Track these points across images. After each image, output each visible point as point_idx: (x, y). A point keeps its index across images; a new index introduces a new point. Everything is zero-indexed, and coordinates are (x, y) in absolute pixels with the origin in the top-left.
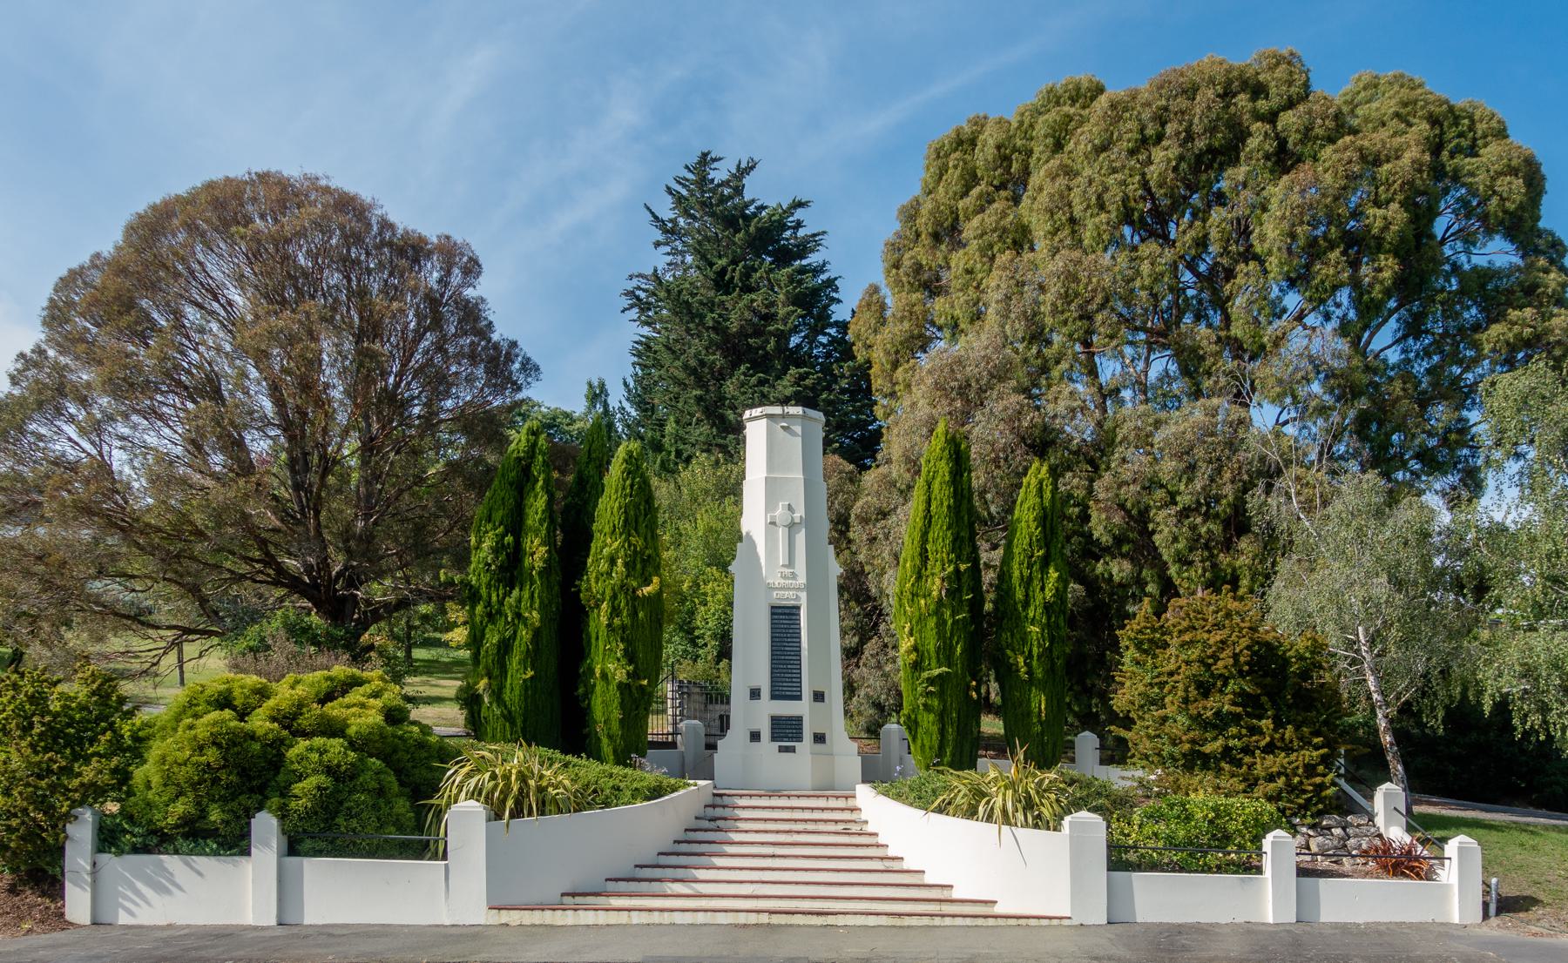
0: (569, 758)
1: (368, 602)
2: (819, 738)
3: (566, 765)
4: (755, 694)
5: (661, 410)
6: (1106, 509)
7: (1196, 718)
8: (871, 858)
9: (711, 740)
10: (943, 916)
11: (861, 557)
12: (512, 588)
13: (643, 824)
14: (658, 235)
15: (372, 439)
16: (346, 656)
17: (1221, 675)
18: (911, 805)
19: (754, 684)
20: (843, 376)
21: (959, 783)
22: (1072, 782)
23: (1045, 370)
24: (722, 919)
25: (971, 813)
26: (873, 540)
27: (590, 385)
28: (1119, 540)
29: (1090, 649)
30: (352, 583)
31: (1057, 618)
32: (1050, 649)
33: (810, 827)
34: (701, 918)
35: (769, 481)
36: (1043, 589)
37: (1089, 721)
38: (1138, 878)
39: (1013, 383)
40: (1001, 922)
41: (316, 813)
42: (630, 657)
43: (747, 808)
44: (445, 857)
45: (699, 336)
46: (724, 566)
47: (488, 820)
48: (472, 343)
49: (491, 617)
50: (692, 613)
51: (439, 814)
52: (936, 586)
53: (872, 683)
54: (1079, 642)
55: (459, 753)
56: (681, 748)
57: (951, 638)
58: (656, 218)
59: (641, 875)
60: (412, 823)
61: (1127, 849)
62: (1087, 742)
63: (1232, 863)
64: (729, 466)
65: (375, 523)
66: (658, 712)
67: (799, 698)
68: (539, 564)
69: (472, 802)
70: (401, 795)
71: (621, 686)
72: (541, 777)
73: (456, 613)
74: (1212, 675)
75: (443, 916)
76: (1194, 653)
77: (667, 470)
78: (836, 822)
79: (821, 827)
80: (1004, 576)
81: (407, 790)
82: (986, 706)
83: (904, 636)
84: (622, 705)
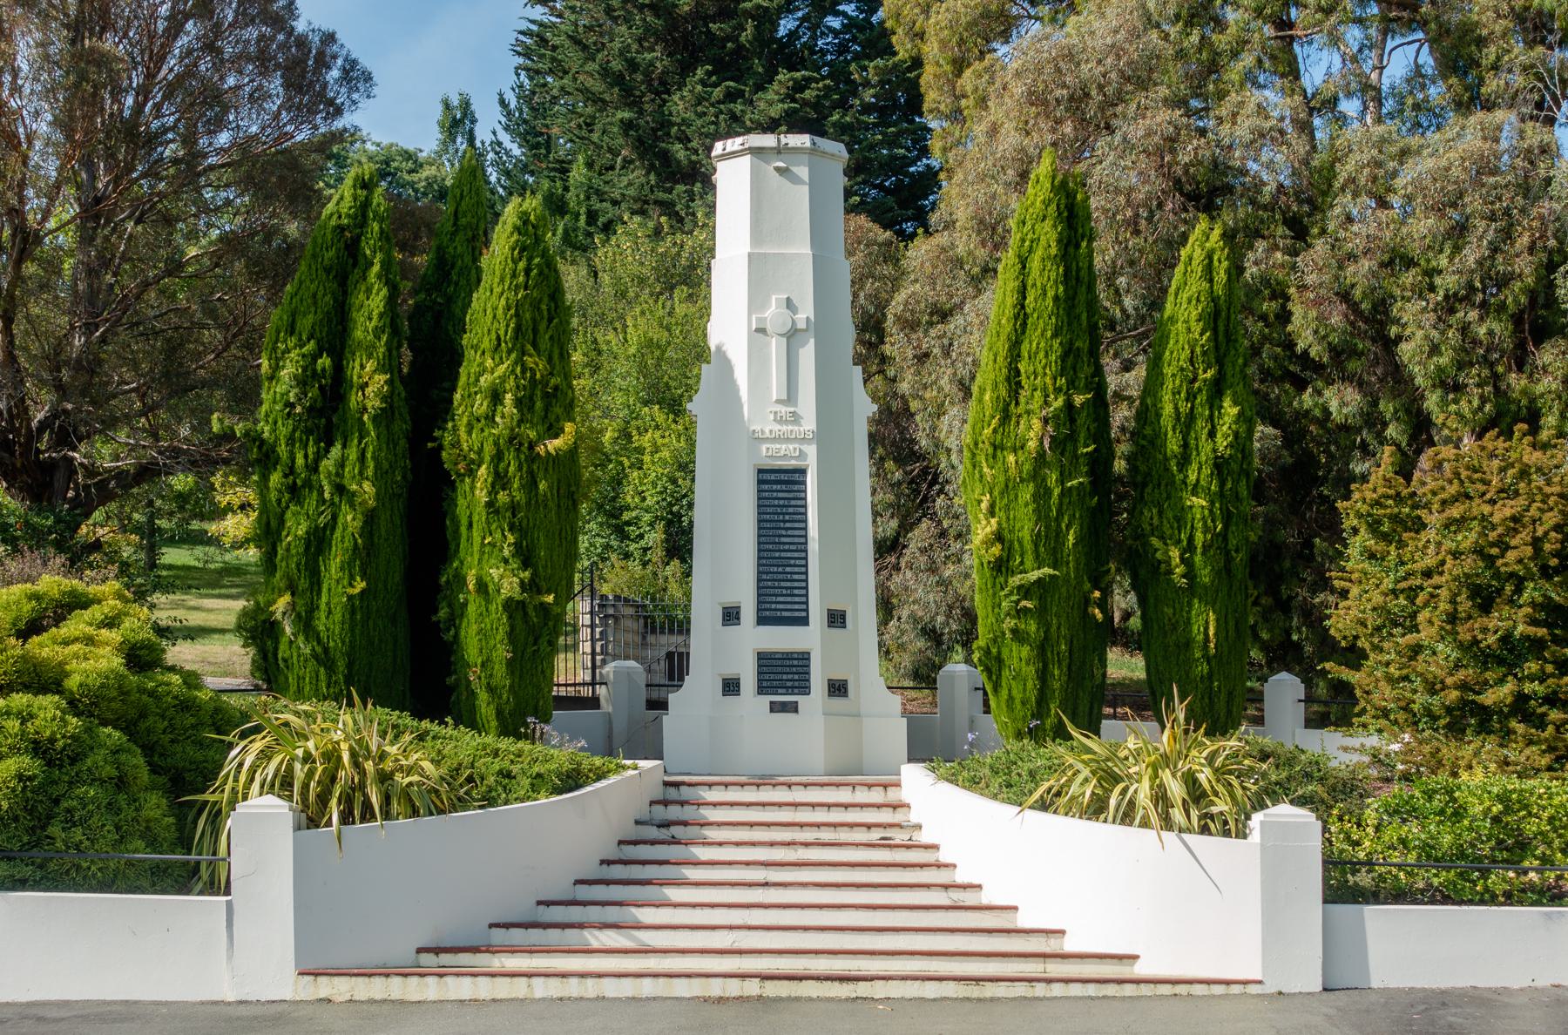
0: (425, 724)
1: (90, 471)
2: (838, 688)
3: (421, 738)
4: (731, 616)
5: (563, 146)
6: (1317, 303)
7: (1471, 648)
8: (928, 886)
9: (655, 695)
10: (1049, 981)
11: (904, 387)
12: (330, 444)
13: (552, 833)
15: (97, 201)
16: (60, 560)
17: (1512, 575)
18: (995, 797)
19: (730, 600)
20: (867, 84)
21: (1076, 760)
22: (1264, 756)
23: (1213, 67)
24: (682, 988)
25: (1096, 809)
26: (923, 357)
27: (447, 105)
28: (1340, 354)
29: (1289, 536)
30: (66, 436)
31: (1236, 482)
32: (1224, 535)
33: (826, 835)
34: (647, 987)
36: (1212, 434)
37: (1284, 655)
38: (1374, 915)
39: (1163, 91)
40: (1145, 990)
41: (16, 819)
42: (525, 555)
43: (720, 805)
44: (227, 893)
45: (627, 20)
46: (675, 407)
47: (298, 828)
48: (262, 37)
49: (295, 491)
50: (618, 482)
51: (217, 818)
52: (1032, 432)
53: (921, 597)
54: (1270, 522)
55: (246, 717)
56: (606, 706)
57: (1058, 519)
59: (548, 917)
60: (172, 835)
61: (1355, 866)
62: (1284, 690)
63: (1531, 887)
64: (679, 237)
65: (103, 340)
66: (566, 649)
67: (804, 621)
68: (373, 403)
69: (270, 799)
70: (152, 787)
71: (510, 606)
72: (383, 756)
73: (230, 491)
74: (1497, 575)
75: (222, 981)
76: (1467, 539)
77: (577, 245)
78: (869, 826)
79: (844, 835)
80: (1146, 413)
81: (162, 779)
82: (1112, 634)
83: (979, 515)
84: (511, 635)
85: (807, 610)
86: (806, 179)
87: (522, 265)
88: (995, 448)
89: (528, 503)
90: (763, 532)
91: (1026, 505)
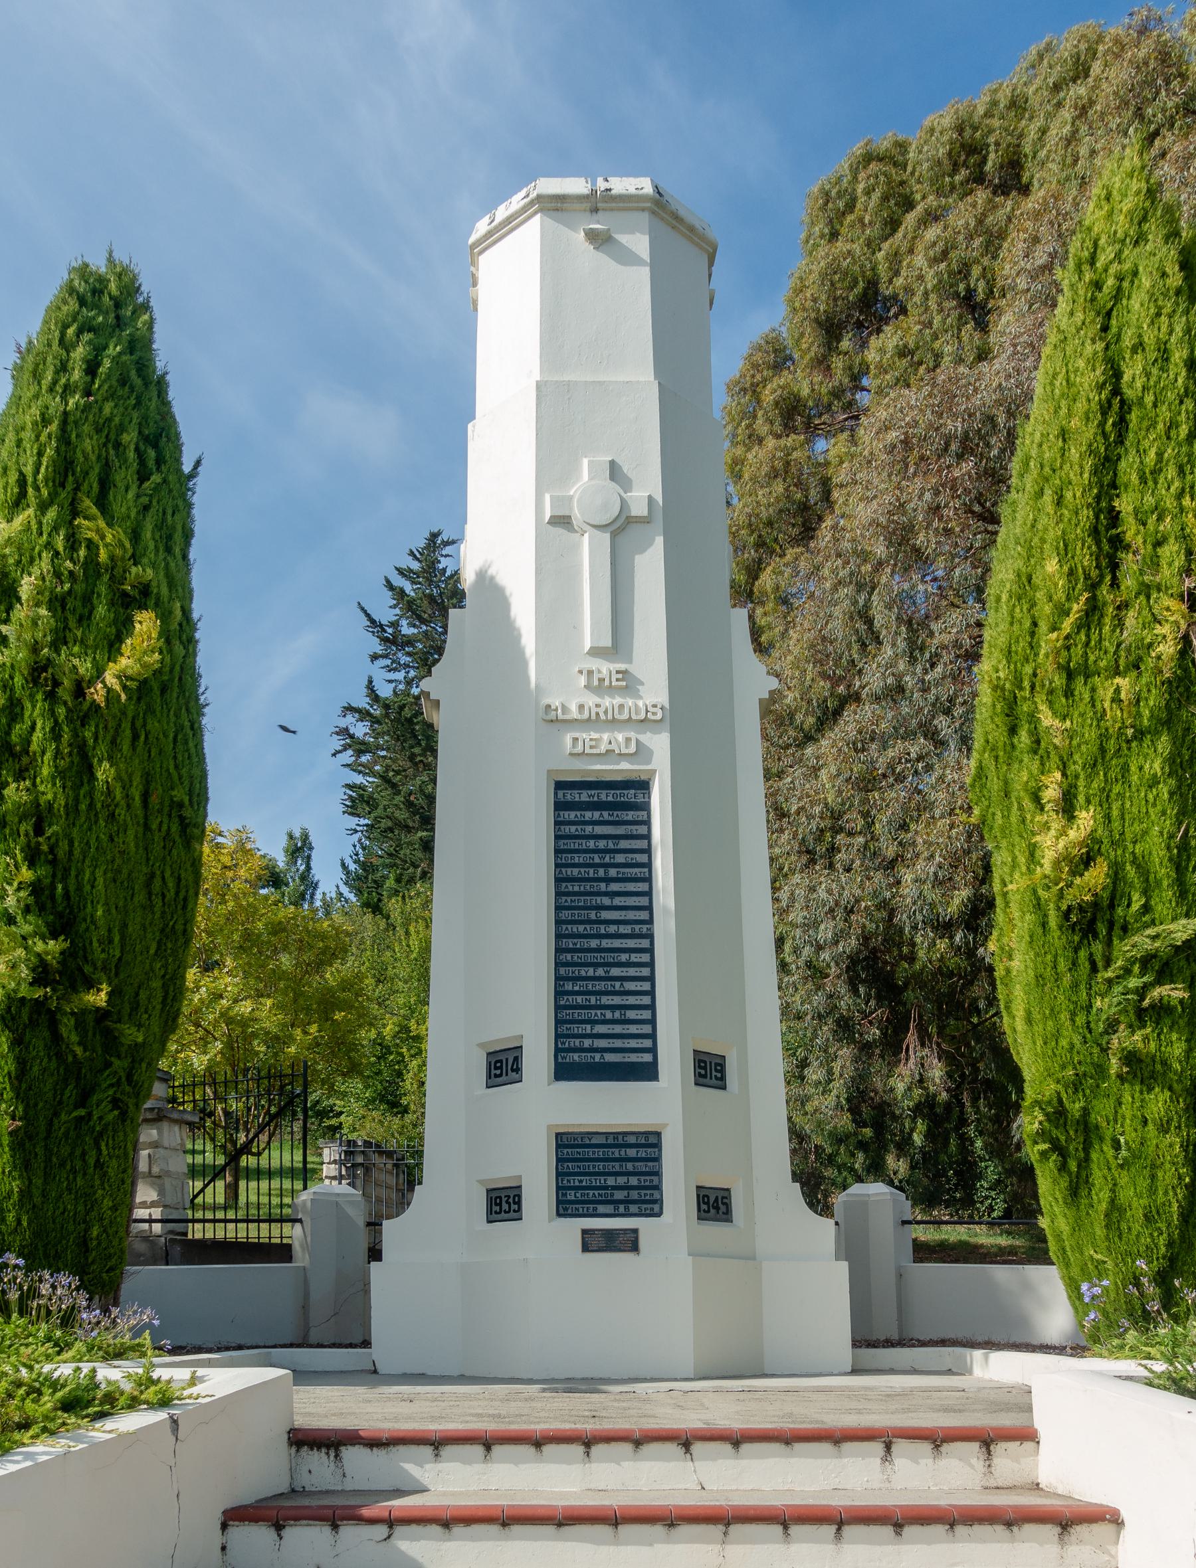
2: (714, 1205)
4: (503, 1066)
14: (377, 647)
27: (291, 837)
35: (550, 395)
56: (301, 1258)
58: (373, 621)
67: (648, 1072)
85: (653, 1050)
86: (646, 256)
87: (79, 352)
88: (1070, 675)
89: (72, 809)
90: (566, 901)
91: (1154, 782)
